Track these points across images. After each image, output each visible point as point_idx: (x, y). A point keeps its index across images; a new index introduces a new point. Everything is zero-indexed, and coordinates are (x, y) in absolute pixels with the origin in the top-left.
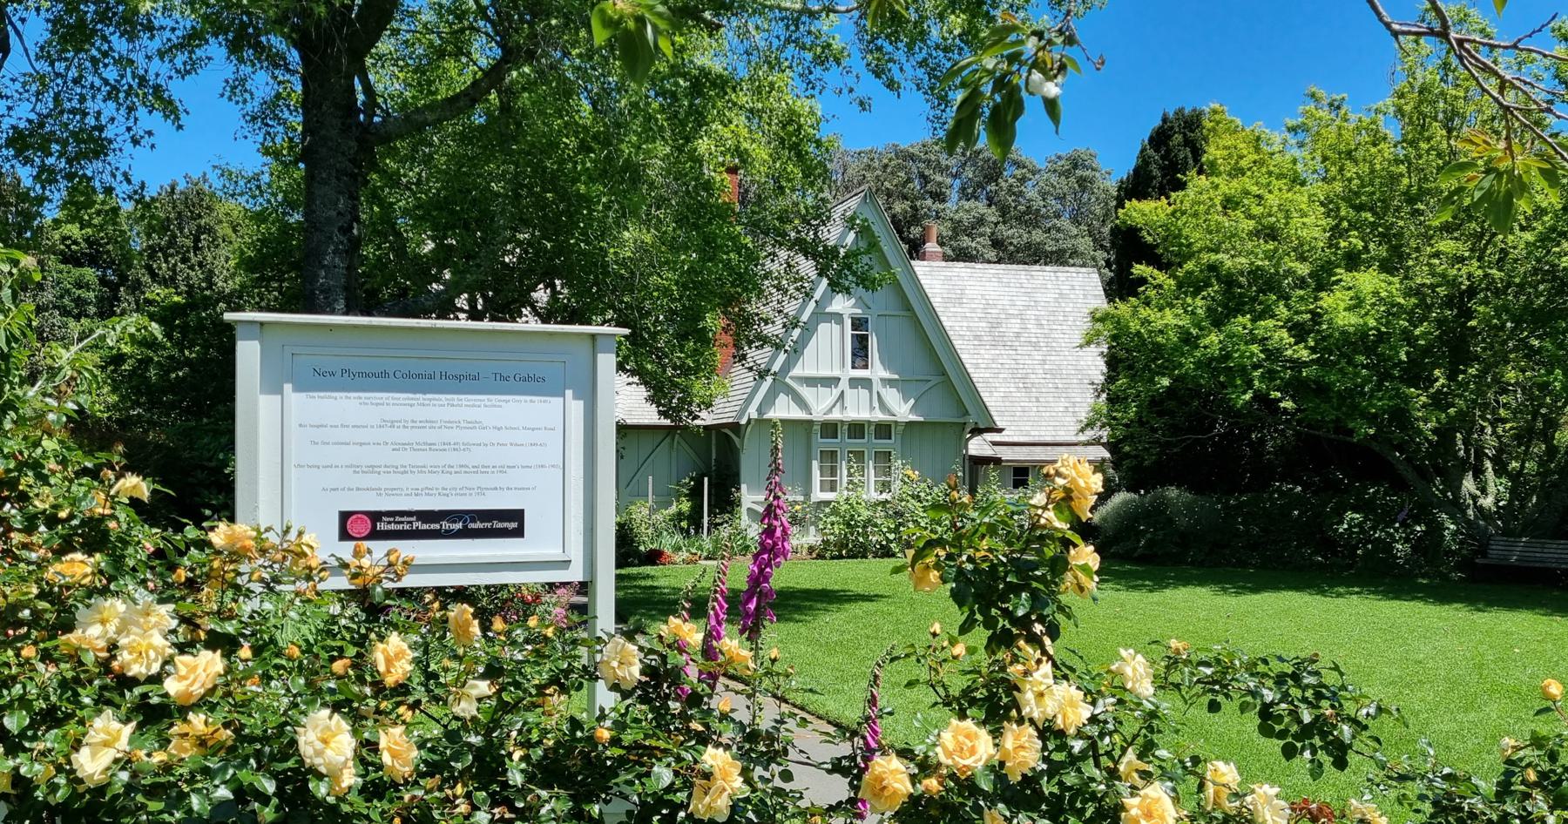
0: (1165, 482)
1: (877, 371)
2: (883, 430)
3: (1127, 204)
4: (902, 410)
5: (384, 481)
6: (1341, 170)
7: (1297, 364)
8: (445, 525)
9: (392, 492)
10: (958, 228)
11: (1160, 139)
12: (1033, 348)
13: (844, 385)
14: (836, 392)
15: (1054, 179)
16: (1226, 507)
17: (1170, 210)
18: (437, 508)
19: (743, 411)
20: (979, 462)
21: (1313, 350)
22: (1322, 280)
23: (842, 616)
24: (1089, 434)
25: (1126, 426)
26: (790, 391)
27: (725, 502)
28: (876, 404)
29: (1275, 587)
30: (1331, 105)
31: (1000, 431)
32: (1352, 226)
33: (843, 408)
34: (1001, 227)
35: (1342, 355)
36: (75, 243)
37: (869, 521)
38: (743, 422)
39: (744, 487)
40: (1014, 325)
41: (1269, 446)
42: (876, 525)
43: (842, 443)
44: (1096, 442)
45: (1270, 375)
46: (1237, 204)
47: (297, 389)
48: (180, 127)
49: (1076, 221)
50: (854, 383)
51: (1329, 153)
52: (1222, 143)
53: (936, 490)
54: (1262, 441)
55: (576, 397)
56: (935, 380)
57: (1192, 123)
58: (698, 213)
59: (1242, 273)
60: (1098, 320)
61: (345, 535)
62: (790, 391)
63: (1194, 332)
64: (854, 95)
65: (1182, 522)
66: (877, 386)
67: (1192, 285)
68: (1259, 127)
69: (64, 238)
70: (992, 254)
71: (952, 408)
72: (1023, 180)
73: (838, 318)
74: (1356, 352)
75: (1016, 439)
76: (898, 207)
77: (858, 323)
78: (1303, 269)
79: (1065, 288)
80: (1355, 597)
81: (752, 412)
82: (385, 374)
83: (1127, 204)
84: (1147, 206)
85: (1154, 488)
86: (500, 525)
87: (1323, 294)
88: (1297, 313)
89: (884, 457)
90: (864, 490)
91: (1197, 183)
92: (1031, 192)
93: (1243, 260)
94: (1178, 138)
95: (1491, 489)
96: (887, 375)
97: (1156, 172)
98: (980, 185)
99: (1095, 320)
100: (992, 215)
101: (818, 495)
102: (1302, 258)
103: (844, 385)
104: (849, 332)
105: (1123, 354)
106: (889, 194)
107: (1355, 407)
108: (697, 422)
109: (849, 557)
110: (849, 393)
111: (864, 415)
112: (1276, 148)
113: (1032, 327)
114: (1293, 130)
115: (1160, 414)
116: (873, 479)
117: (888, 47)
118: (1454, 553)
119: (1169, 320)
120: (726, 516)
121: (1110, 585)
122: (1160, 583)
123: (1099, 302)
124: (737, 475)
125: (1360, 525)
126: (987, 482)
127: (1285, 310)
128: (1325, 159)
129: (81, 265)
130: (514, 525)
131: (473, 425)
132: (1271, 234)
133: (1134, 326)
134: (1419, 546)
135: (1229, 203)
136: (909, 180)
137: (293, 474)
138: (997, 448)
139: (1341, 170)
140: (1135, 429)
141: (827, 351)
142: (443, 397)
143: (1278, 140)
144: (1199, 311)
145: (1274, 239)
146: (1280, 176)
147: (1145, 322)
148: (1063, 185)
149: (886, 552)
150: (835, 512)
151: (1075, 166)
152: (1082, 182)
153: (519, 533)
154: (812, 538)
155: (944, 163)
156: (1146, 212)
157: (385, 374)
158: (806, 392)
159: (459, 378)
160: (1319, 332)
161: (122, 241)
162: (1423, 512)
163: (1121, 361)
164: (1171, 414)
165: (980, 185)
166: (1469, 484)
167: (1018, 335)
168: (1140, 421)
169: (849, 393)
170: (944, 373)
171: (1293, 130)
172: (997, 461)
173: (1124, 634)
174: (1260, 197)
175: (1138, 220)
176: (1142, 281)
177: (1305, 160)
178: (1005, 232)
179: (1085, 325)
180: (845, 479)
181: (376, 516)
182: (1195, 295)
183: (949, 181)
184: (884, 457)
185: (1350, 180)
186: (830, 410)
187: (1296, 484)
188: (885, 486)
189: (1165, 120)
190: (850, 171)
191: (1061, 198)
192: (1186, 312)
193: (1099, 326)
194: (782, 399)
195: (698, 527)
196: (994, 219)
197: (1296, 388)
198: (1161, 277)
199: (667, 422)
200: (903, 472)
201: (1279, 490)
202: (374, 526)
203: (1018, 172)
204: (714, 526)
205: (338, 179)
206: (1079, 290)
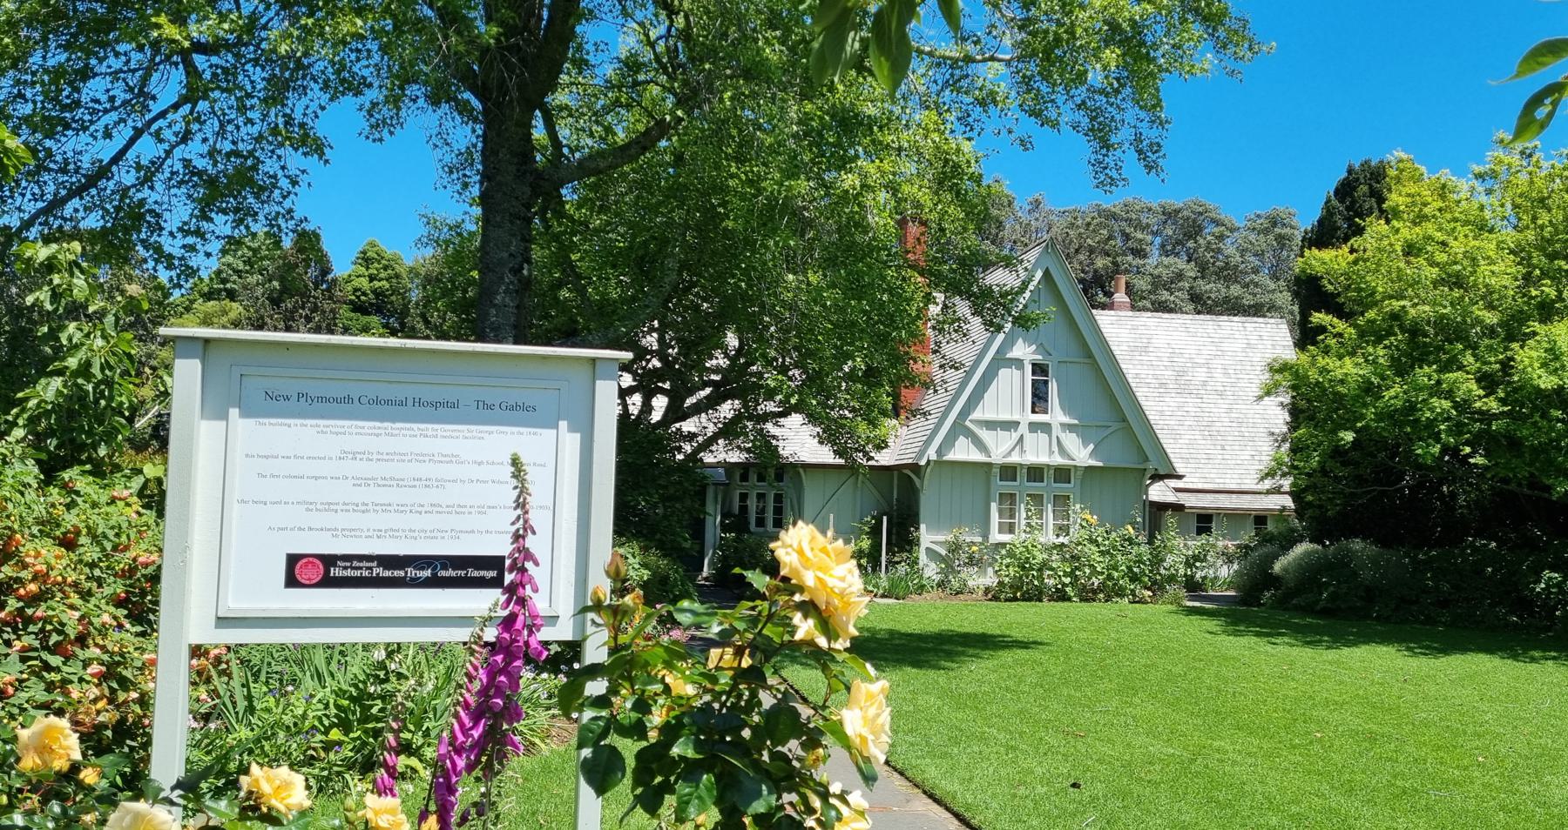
0: (1351, 533)
1: (1056, 415)
2: (1062, 474)
3: (1307, 253)
4: (1081, 454)
5: (341, 520)
6: (1534, 219)
7: (1486, 417)
8: (411, 572)
9: (350, 532)
10: (1157, 283)
11: (1345, 190)
13: (1023, 429)
14: (1015, 436)
15: (1252, 237)
16: (1414, 560)
17: (1351, 258)
20: (1161, 507)
21: (1503, 401)
22: (1513, 330)
23: (990, 664)
24: (1268, 484)
25: (1308, 475)
26: (970, 434)
28: (1055, 448)
29: (1464, 649)
30: (1522, 153)
31: (1180, 477)
32: (1544, 274)
33: (1022, 451)
34: (1200, 282)
35: (1535, 408)
36: (364, 294)
37: (1044, 565)
38: (923, 463)
39: (923, 527)
40: (1201, 374)
41: (1461, 500)
42: (1052, 569)
43: (1021, 485)
44: (1277, 491)
45: (1457, 429)
46: (1420, 250)
47: (245, 414)
48: (327, 161)
49: (1275, 277)
50: (1034, 427)
51: (1518, 201)
52: (1405, 191)
53: (1114, 535)
55: (572, 429)
56: (1116, 426)
57: (1376, 175)
58: (850, 253)
59: (1428, 323)
60: (1277, 371)
61: (292, 581)
62: (970, 434)
63: (1375, 380)
64: (1013, 136)
65: (1366, 575)
67: (1374, 334)
68: (1445, 175)
69: (356, 290)
70: (1191, 307)
71: (1132, 453)
72: (1221, 238)
73: (1018, 363)
74: (1550, 405)
75: (1200, 486)
77: (1039, 369)
78: (1491, 318)
79: (1253, 339)
80: (1550, 663)
81: (931, 453)
82: (349, 399)
83: (1307, 253)
84: (1327, 254)
85: (1338, 540)
86: (476, 574)
87: (1515, 346)
88: (1485, 363)
89: (1061, 501)
90: (1039, 533)
91: (1376, 227)
92: (1229, 249)
93: (1427, 308)
94: (1364, 188)
96: (1067, 420)
98: (1179, 242)
99: (1271, 370)
100: (1191, 270)
101: (996, 537)
102: (1490, 307)
103: (1023, 429)
104: (1029, 377)
105: (1303, 404)
106: (1092, 251)
107: (1551, 462)
108: (871, 463)
109: (1024, 600)
112: (1463, 195)
114: (1479, 176)
115: (1344, 464)
116: (1051, 521)
117: (1044, 89)
119: (1349, 369)
120: (905, 555)
121: (1286, 639)
122: (1340, 639)
123: (1289, 353)
124: (917, 515)
125: (1559, 585)
127: (1471, 360)
128: (1515, 206)
129: (369, 314)
130: (492, 574)
131: (452, 459)
132: (1457, 282)
133: (1313, 375)
135: (1410, 250)
136: (1110, 238)
137: (235, 511)
138: (1180, 495)
139: (1534, 219)
141: (1008, 394)
143: (1465, 187)
144: (1381, 361)
145: (1460, 287)
146: (1466, 223)
147: (1324, 371)
148: (1261, 242)
149: (1061, 596)
150: (1011, 554)
151: (1274, 224)
154: (989, 579)
155: (1145, 221)
156: (1330, 261)
157: (349, 399)
158: (985, 435)
159: (435, 405)
160: (1509, 383)
161: (403, 294)
163: (1302, 411)
164: (1356, 464)
165: (1179, 242)
167: (1205, 383)
168: (1323, 470)
170: (1124, 420)
171: (1479, 176)
172: (1178, 508)
173: (1286, 696)
174: (1444, 244)
175: (1319, 269)
176: (1322, 329)
177: (1494, 206)
178: (1203, 286)
180: (1023, 522)
181: (329, 560)
183: (1149, 238)
184: (1061, 501)
185: (1542, 227)
186: (1009, 454)
187: (1490, 539)
188: (1062, 530)
189: (1350, 171)
190: (1054, 229)
191: (1259, 255)
192: (1367, 361)
193: (1278, 377)
194: (962, 441)
196: (1193, 274)
198: (1341, 326)
199: (842, 461)
200: (1081, 515)
201: (1472, 545)
202: (327, 571)
203: (1216, 230)
204: (891, 563)
205: (512, 223)
206: (1272, 338)
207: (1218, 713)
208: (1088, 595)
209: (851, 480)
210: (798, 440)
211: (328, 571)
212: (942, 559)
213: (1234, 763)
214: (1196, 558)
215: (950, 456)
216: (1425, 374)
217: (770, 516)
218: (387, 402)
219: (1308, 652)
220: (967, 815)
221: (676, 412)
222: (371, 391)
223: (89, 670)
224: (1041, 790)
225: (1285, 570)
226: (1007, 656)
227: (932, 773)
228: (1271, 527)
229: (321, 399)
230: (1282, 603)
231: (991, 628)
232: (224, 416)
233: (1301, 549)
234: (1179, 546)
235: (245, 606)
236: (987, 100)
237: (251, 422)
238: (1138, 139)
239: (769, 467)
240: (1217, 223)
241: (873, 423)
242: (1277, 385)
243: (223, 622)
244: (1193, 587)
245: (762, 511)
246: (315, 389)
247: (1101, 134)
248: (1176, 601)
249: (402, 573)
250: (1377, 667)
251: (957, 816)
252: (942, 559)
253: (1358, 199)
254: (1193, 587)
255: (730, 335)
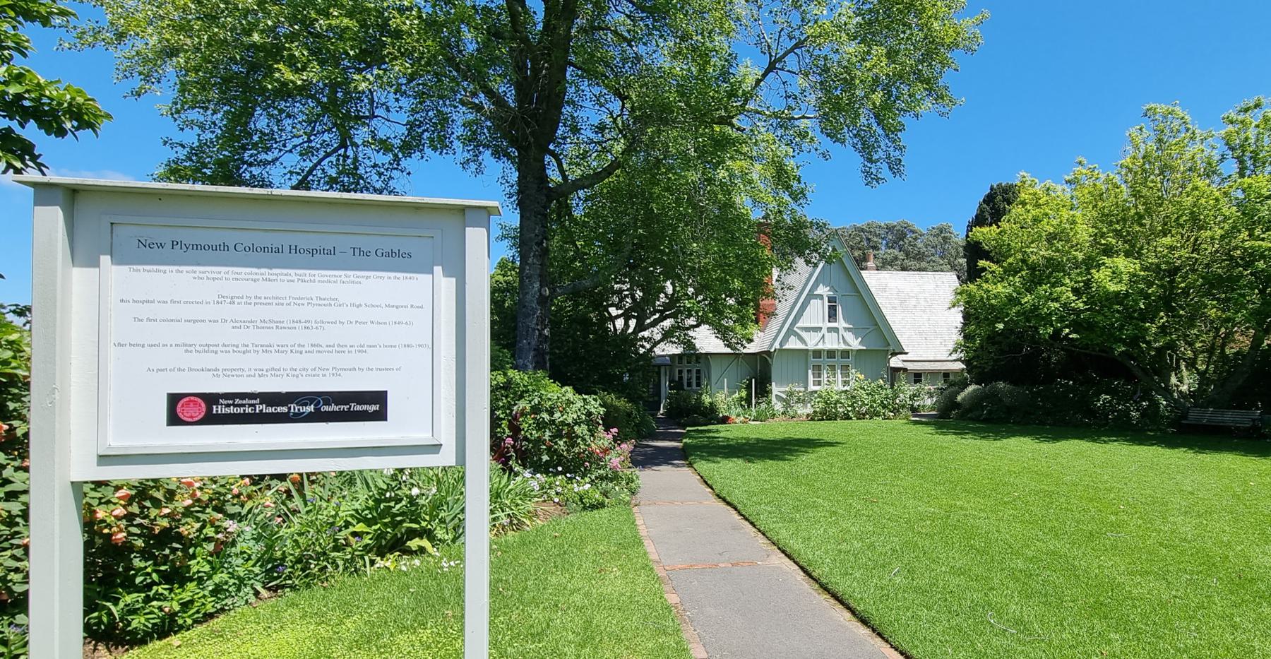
1: (841, 323)
2: (846, 354)
4: (855, 343)
5: (222, 361)
7: (1078, 312)
8: (294, 408)
11: (989, 199)
12: (926, 316)
13: (824, 331)
14: (820, 335)
16: (1031, 391)
18: (284, 390)
19: (772, 345)
20: (896, 370)
22: (1090, 264)
23: (813, 456)
24: (954, 356)
27: (763, 391)
37: (837, 401)
40: (913, 302)
41: (1054, 359)
43: (824, 361)
44: (959, 360)
47: (118, 260)
50: (830, 330)
54: (1049, 358)
55: (447, 274)
58: (727, 223)
61: (174, 419)
68: (1049, 183)
72: (916, 239)
73: (821, 297)
76: (856, 254)
79: (939, 283)
82: (225, 247)
84: (985, 229)
86: (359, 408)
87: (1093, 271)
89: (845, 368)
90: (834, 385)
91: (1016, 210)
95: (1186, 381)
97: (987, 216)
99: (957, 294)
100: (901, 255)
101: (812, 388)
103: (824, 331)
104: (827, 304)
110: (827, 335)
111: (835, 346)
113: (923, 303)
115: (993, 344)
118: (1168, 417)
122: (999, 435)
126: (900, 380)
130: (375, 408)
134: (1144, 414)
140: (980, 352)
141: (816, 313)
142: (292, 272)
149: (846, 417)
150: (820, 396)
152: (945, 239)
153: (381, 415)
154: (809, 410)
158: (804, 334)
159: (312, 252)
162: (1146, 395)
164: (1000, 343)
166: (1173, 380)
168: (982, 347)
169: (827, 335)
172: (905, 370)
176: (984, 269)
179: (951, 297)
181: (211, 399)
182: (1014, 276)
184: (845, 368)
188: (846, 383)
189: (992, 189)
195: (749, 404)
197: (1076, 326)
198: (994, 267)
199: (729, 350)
200: (856, 376)
202: (209, 409)
206: (945, 283)
207: (951, 482)
208: (861, 416)
210: (706, 340)
211: (213, 409)
212: (784, 400)
213: (975, 517)
214: (914, 395)
216: (1043, 289)
217: (694, 381)
218: (263, 249)
219: (985, 443)
220: (810, 569)
221: (641, 327)
222: (247, 239)
223: (117, 495)
224: (857, 545)
225: (963, 399)
226: (823, 451)
227: (783, 535)
228: (951, 377)
229: (196, 247)
230: (962, 417)
231: (812, 436)
232: (96, 264)
233: (971, 388)
234: (907, 389)
235: (126, 444)
236: (803, 135)
237: (125, 269)
238: (889, 157)
239: (692, 356)
240: (913, 232)
241: (744, 326)
242: (958, 301)
243: (104, 459)
244: (914, 410)
245: (689, 379)
246: (188, 237)
247: (867, 149)
248: (906, 418)
249: (285, 409)
250: (1021, 452)
251: (802, 568)
252: (784, 400)
253: (995, 205)
254: (914, 410)
255: (471, 48)
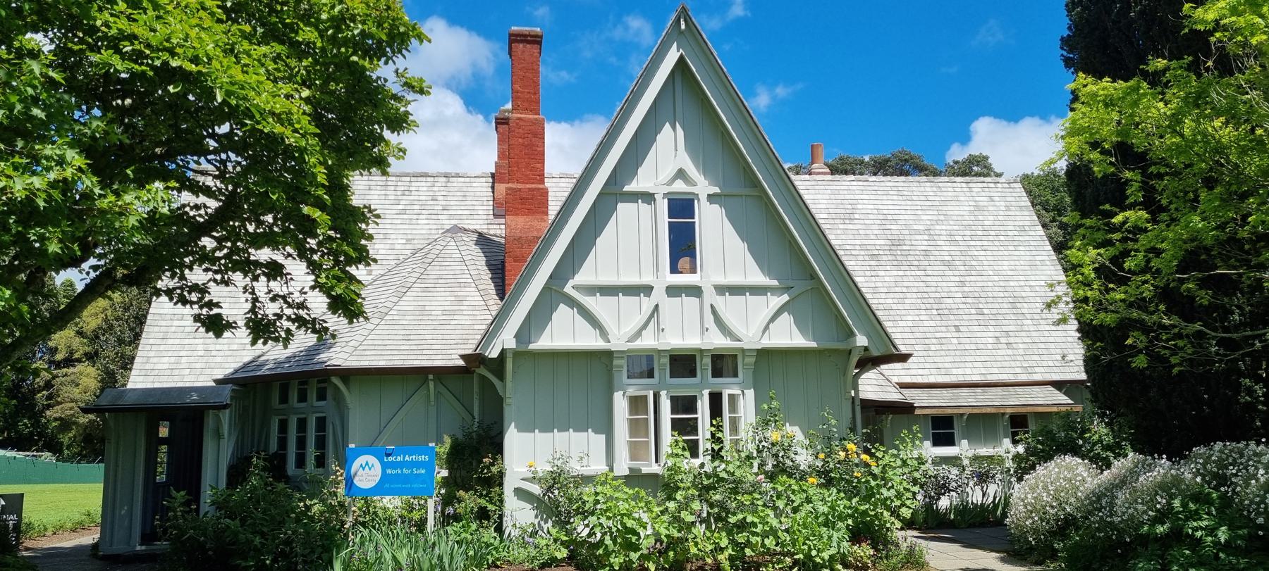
13: (659, 295)
14: (647, 304)
26: (572, 303)
31: (904, 358)
40: (921, 243)
50: (673, 291)
62: (572, 303)
66: (710, 296)
75: (932, 380)
79: (983, 202)
104: (664, 220)
110: (670, 306)
138: (904, 391)
158: (593, 303)
167: (926, 253)
172: (904, 409)
186: (638, 334)
194: (563, 313)
209: (422, 392)
215: (547, 341)
217: (311, 453)
